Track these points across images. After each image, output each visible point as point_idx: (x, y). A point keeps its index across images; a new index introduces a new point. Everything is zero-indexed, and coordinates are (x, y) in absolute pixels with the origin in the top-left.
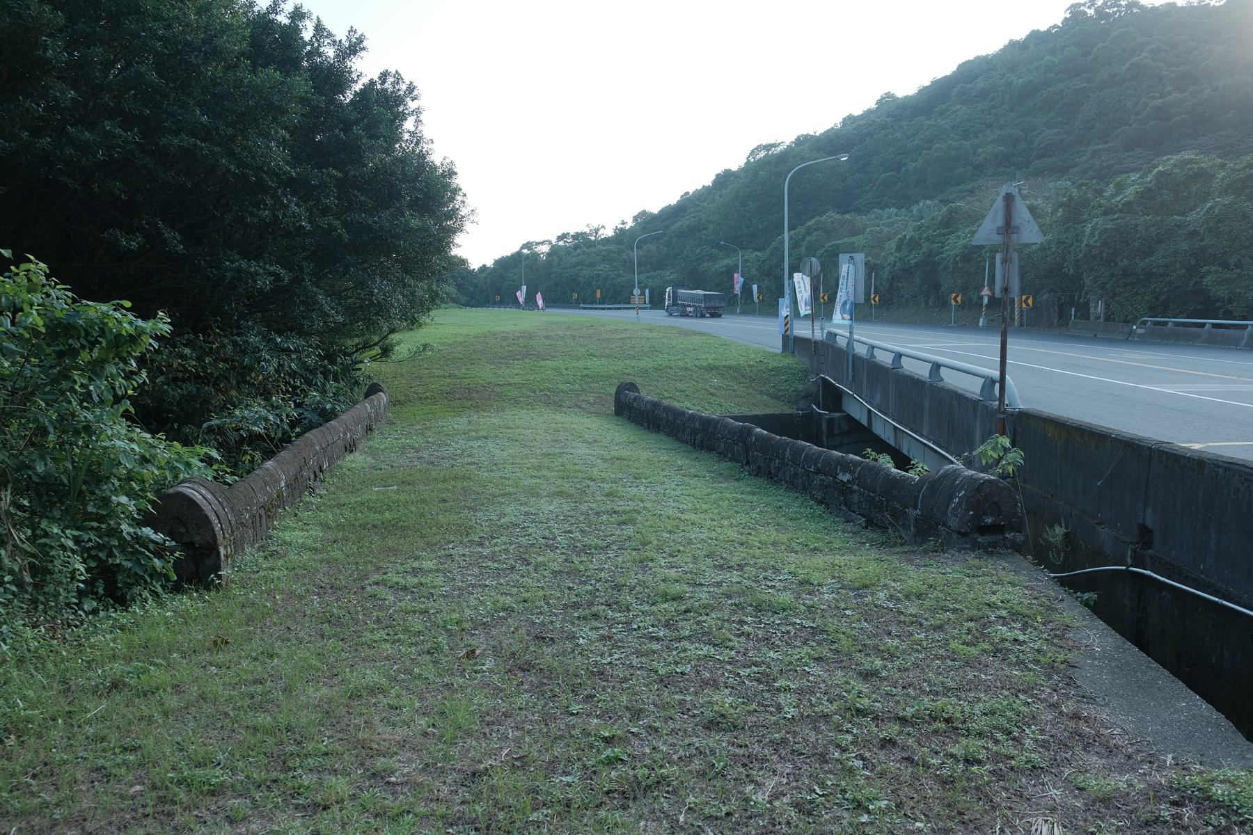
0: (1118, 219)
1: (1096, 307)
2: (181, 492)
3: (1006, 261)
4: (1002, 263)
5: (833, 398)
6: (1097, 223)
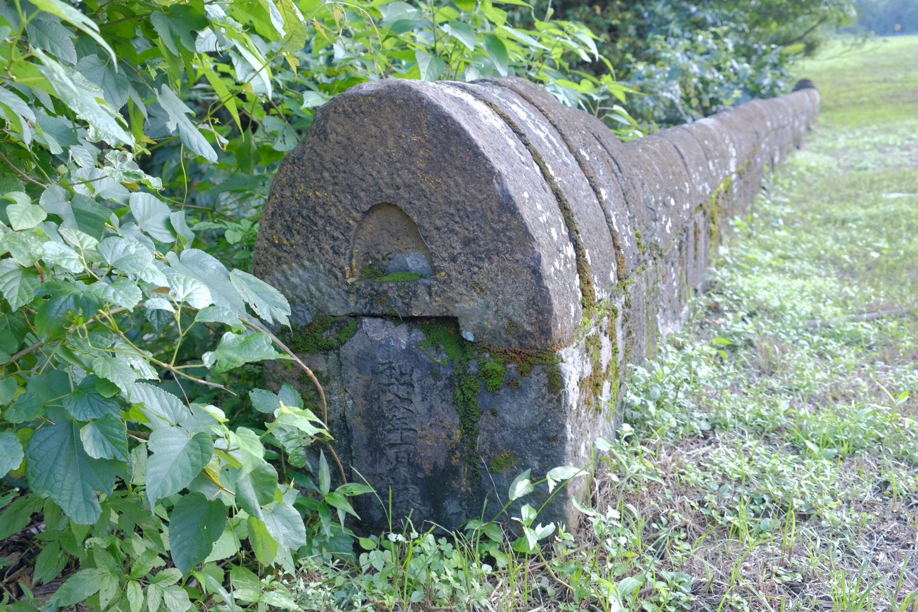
2: (403, 87)
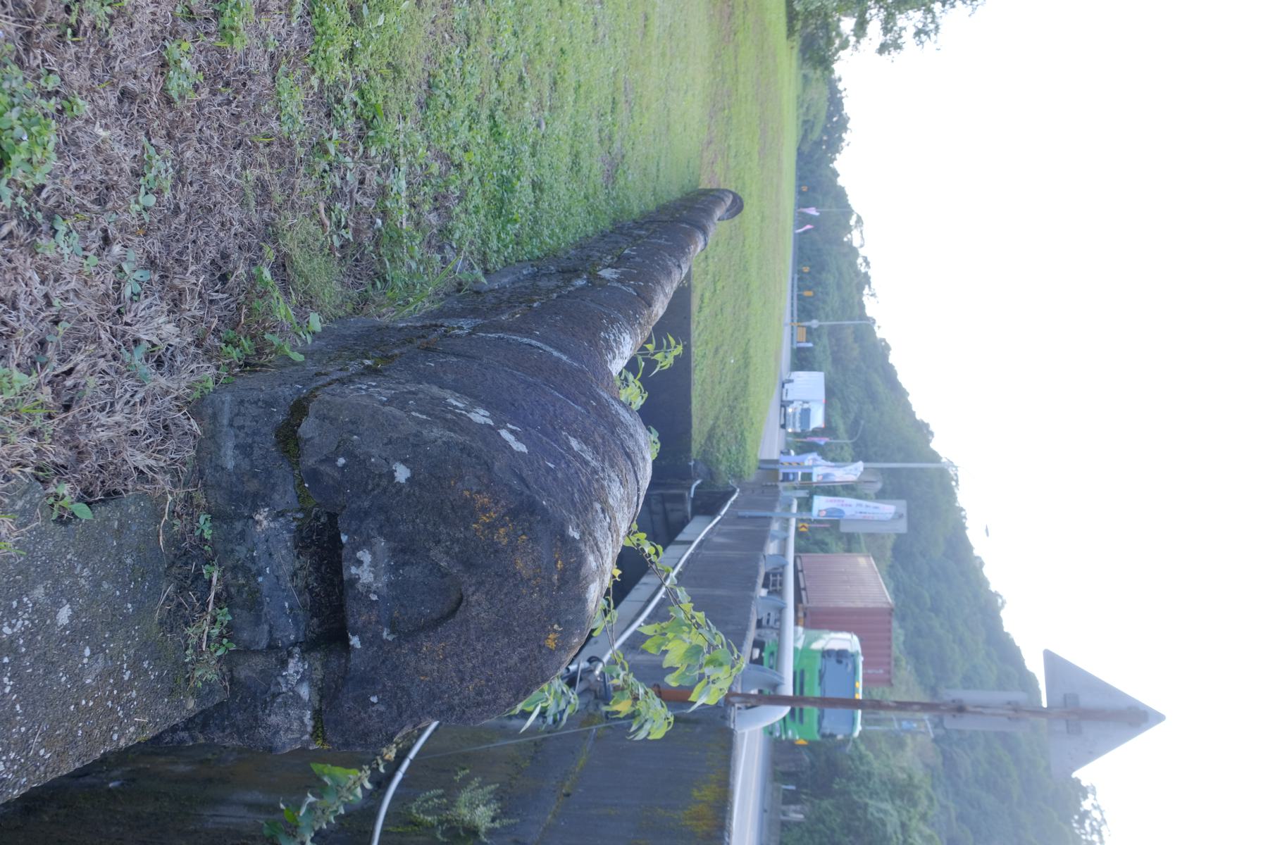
0: (897, 838)
1: (796, 812)
3: (1015, 710)
4: (1009, 703)
5: (708, 505)
6: (892, 815)
